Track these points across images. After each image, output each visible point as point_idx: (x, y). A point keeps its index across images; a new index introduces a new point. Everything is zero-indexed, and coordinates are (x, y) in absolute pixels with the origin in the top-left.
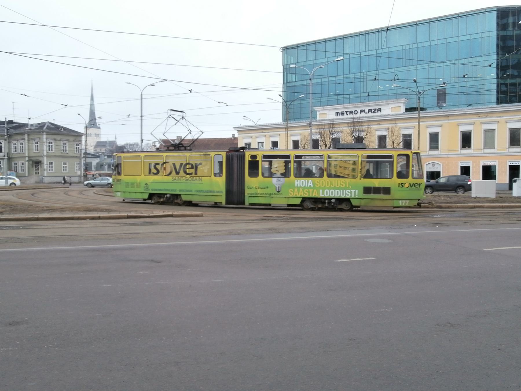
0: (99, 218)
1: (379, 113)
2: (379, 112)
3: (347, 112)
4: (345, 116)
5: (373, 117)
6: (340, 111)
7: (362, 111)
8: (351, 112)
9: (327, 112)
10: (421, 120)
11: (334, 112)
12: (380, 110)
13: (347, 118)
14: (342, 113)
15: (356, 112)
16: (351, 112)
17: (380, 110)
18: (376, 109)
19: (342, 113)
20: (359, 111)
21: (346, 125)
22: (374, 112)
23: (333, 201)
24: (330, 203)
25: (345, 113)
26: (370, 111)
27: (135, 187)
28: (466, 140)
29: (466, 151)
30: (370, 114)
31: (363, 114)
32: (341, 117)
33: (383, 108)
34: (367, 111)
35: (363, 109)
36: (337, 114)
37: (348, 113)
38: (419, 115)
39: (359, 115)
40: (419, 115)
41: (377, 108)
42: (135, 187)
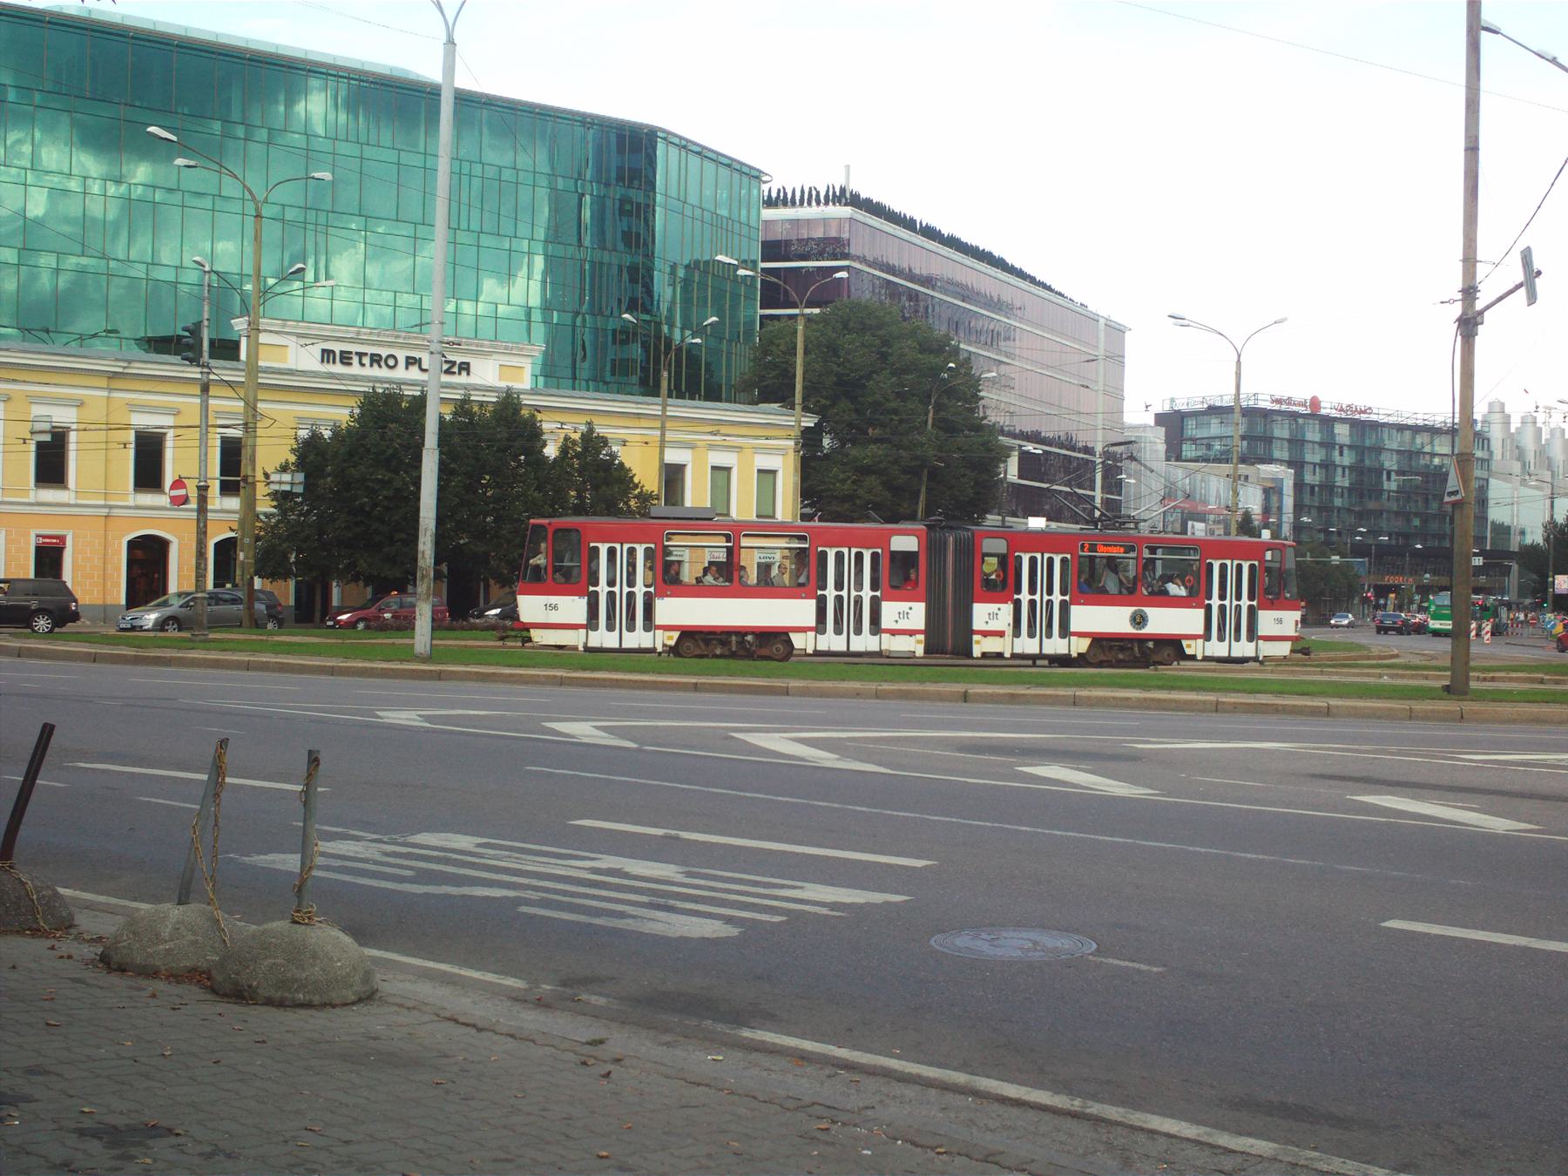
1: (462, 379)
2: (464, 373)
3: (361, 355)
4: (355, 369)
6: (337, 347)
7: (411, 361)
8: (376, 359)
9: (291, 342)
10: (30, 189)
11: (316, 351)
12: (465, 367)
13: (355, 378)
14: (345, 358)
15: (389, 362)
16: (376, 359)
17: (465, 367)
18: (454, 363)
19: (345, 358)
20: (402, 362)
21: (103, 383)
23: (749, 638)
24: (741, 643)
25: (355, 360)
27: (182, 492)
28: (51, 464)
29: (50, 495)
32: (338, 368)
35: (416, 354)
36: (327, 355)
37: (366, 360)
38: (664, 410)
39: (400, 373)
40: (664, 410)
42: (182, 492)
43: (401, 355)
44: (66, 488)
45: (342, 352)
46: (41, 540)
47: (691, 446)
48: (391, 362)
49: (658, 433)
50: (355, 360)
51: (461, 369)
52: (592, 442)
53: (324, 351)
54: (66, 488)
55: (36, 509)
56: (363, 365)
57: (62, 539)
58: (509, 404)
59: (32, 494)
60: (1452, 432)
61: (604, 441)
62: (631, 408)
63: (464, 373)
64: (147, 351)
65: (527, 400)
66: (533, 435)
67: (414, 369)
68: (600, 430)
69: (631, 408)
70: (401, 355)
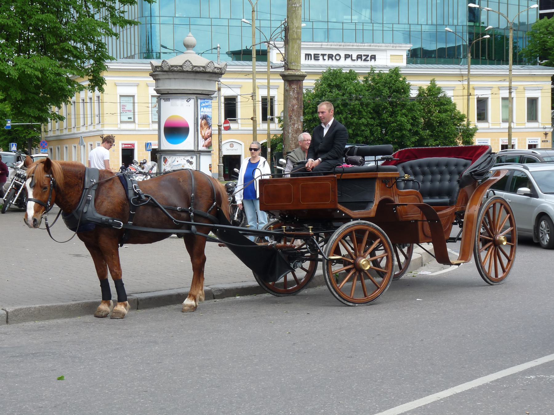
0: (130, 130)
1: (372, 63)
2: (373, 60)
3: (323, 55)
4: (321, 62)
5: (361, 67)
6: (312, 52)
7: (347, 56)
8: (330, 57)
12: (373, 57)
13: (321, 66)
14: (316, 57)
16: (330, 57)
17: (373, 57)
18: (368, 56)
19: (316, 57)
22: (365, 60)
25: (321, 58)
26: (359, 57)
30: (359, 63)
31: (349, 62)
32: (313, 62)
33: (378, 55)
34: (354, 57)
35: (350, 53)
38: (469, 71)
39: (342, 63)
40: (469, 71)
41: (370, 53)
43: (342, 54)
44: (487, 121)
45: (315, 55)
46: (124, 146)
47: (490, 88)
48: (338, 58)
49: (267, 81)
50: (321, 58)
51: (371, 58)
52: (433, 91)
53: (306, 55)
54: (487, 121)
55: (135, 133)
56: (324, 60)
57: (133, 145)
58: (395, 72)
59: (119, 126)
60: (161, 67)
61: (439, 90)
62: (527, 72)
63: (373, 60)
64: (237, 60)
65: (402, 71)
66: (405, 89)
67: (349, 60)
68: (439, 84)
69: (527, 72)
70: (342, 54)
